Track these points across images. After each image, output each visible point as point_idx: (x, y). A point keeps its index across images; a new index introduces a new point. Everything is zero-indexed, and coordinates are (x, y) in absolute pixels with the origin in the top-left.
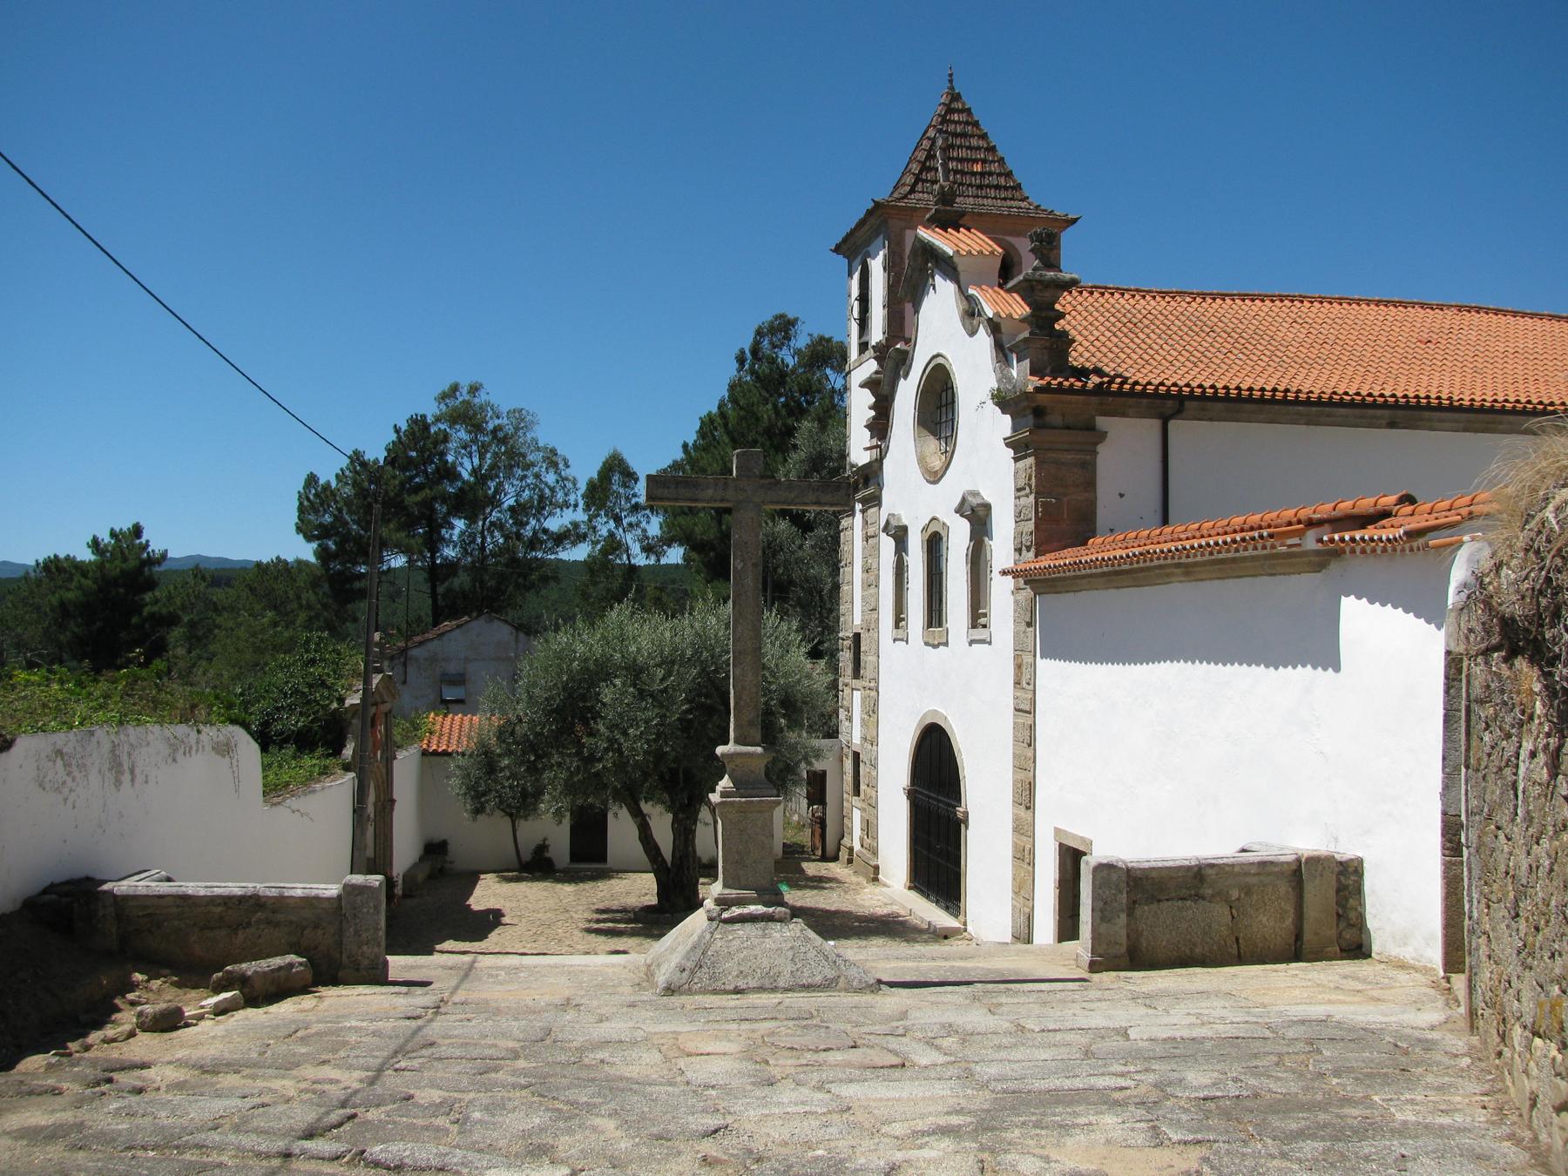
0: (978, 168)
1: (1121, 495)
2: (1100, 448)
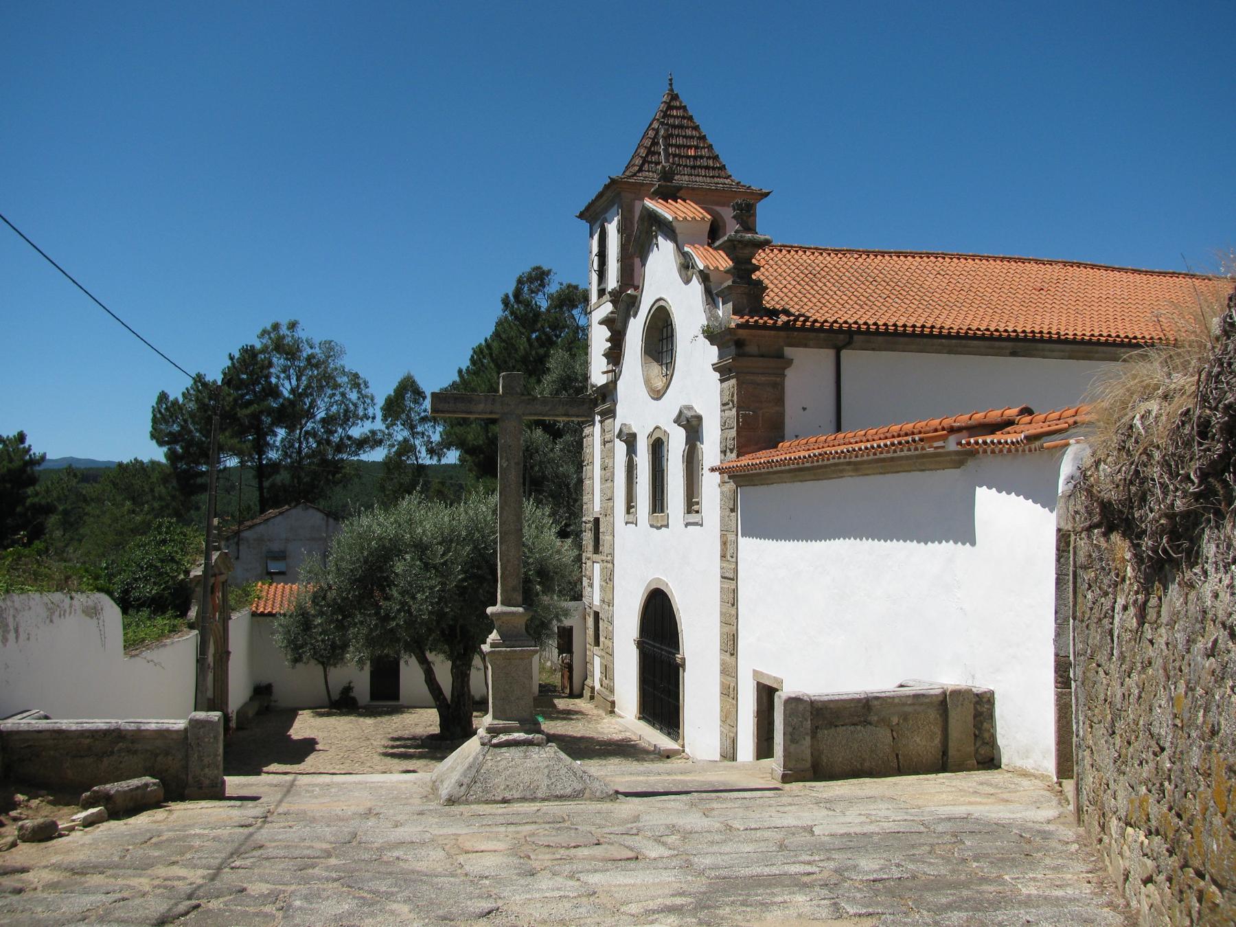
0: (692, 152)
1: (804, 409)
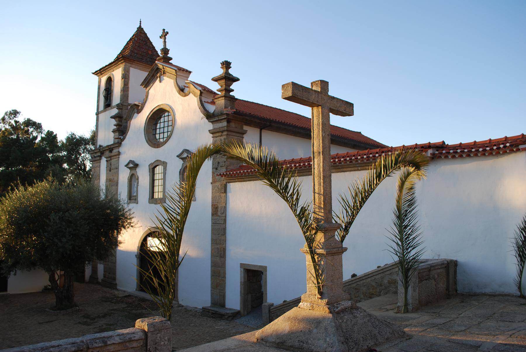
2: (244, 136)
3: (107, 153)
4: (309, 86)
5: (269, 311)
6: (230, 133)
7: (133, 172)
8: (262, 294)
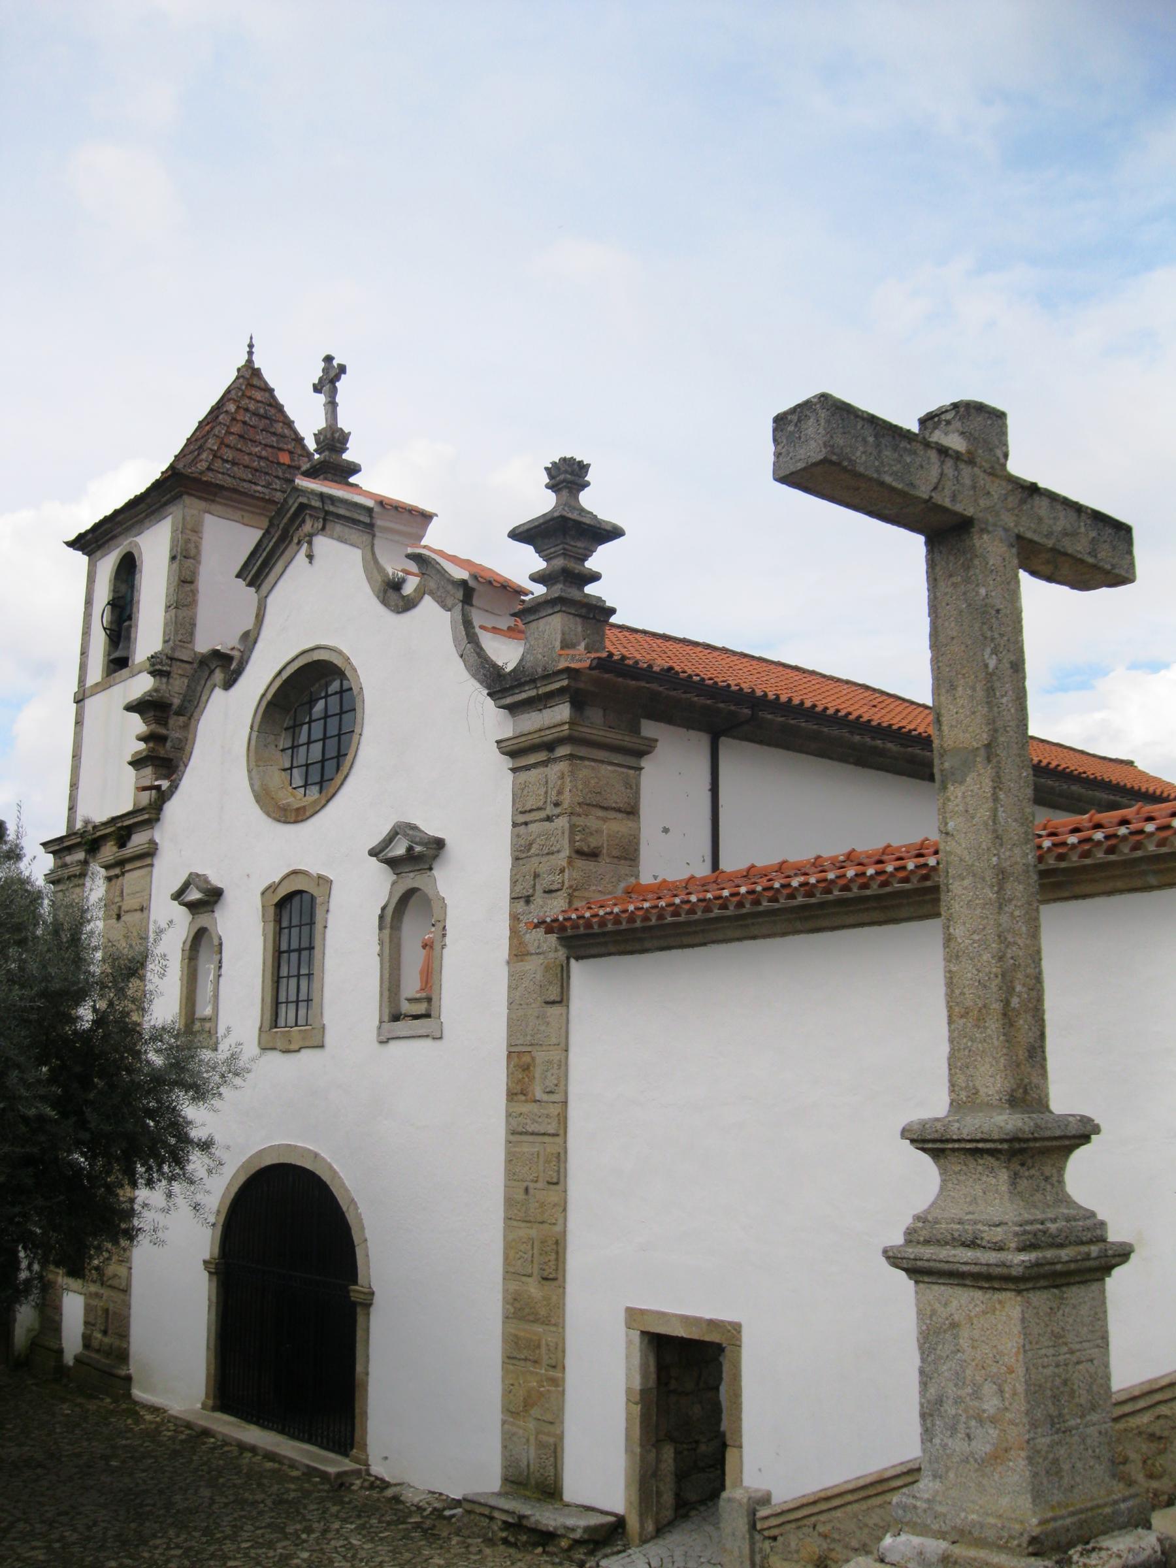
2: (645, 763)
3: (109, 851)
4: (915, 428)
5: (753, 1526)
6: (582, 751)
7: (203, 920)
8: (724, 1446)
